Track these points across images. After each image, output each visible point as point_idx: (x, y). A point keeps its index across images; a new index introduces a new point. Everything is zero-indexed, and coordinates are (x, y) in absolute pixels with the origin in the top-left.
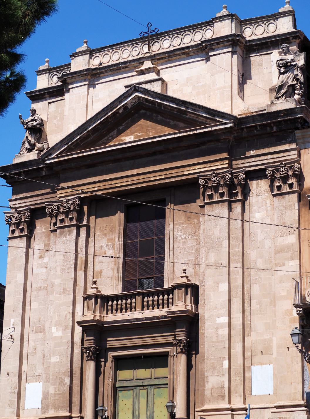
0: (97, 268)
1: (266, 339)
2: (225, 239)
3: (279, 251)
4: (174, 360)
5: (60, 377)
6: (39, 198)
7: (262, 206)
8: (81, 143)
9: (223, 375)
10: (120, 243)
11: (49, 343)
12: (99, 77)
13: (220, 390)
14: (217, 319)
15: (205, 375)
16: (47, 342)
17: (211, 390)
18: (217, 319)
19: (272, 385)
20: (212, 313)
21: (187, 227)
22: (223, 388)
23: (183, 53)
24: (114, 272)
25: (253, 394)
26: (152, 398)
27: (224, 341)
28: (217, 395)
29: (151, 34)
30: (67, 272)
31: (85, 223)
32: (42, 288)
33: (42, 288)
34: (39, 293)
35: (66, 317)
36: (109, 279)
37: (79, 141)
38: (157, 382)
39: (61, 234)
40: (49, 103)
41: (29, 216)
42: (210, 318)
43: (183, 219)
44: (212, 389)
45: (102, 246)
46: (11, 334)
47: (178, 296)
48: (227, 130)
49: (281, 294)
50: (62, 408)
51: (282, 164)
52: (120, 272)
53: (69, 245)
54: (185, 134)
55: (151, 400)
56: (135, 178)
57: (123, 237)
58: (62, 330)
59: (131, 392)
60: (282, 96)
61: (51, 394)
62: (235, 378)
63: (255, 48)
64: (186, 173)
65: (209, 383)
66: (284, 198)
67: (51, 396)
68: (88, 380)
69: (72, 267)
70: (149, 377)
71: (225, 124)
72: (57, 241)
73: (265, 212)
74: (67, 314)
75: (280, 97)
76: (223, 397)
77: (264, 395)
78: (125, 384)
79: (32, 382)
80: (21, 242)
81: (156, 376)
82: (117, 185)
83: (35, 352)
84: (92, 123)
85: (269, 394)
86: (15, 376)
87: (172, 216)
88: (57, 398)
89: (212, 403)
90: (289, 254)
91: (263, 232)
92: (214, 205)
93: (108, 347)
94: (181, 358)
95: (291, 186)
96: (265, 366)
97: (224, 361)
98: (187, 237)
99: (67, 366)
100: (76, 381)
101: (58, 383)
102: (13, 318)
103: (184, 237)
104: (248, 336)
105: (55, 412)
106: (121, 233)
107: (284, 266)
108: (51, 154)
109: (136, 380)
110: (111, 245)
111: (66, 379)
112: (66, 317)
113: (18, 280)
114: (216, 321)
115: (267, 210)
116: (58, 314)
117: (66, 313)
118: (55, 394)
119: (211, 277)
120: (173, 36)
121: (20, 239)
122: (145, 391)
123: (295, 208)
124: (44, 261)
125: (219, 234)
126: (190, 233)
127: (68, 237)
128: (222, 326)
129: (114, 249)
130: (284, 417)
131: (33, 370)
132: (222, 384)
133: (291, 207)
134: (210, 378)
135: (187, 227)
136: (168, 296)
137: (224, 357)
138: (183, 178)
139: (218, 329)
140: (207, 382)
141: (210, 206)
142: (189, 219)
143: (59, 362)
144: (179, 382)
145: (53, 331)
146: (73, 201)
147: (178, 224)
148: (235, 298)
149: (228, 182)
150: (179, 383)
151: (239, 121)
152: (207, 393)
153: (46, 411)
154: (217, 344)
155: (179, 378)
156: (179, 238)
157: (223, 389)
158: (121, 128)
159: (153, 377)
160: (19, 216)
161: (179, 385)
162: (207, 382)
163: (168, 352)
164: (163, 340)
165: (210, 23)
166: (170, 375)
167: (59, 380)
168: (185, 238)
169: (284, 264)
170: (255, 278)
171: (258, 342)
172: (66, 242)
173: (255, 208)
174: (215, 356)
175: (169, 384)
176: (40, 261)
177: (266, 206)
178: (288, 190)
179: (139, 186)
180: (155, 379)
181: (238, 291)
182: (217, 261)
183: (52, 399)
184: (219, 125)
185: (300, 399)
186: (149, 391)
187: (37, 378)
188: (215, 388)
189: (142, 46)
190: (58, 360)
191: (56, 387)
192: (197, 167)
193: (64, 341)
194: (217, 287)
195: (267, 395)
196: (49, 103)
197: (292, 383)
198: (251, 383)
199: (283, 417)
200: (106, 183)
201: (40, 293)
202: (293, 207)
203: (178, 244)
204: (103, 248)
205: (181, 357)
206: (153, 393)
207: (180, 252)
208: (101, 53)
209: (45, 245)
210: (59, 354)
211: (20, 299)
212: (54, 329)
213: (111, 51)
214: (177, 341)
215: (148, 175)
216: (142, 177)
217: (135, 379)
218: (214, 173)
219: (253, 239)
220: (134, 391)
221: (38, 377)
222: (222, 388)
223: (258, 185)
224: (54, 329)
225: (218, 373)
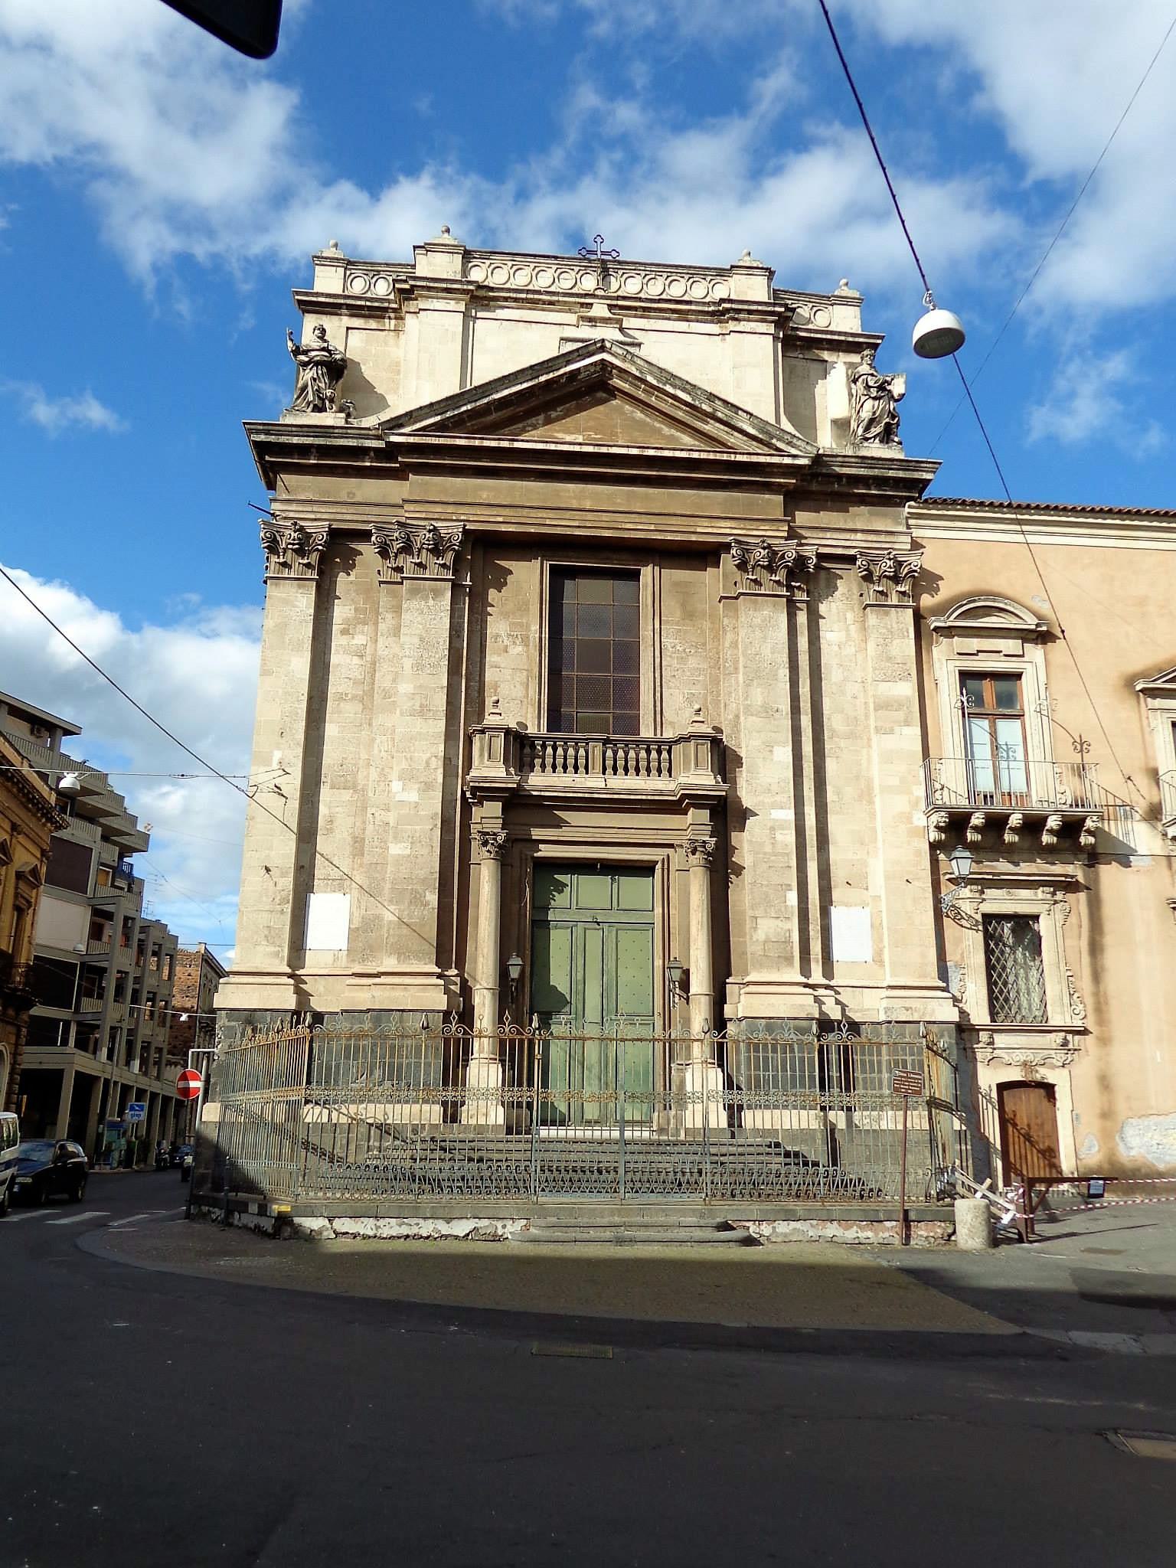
3: (884, 705)
6: (352, 509)
8: (469, 421)
11: (376, 814)
12: (487, 305)
16: (370, 811)
21: (686, 632)
27: (787, 854)
33: (349, 696)
35: (428, 763)
36: (516, 702)
37: (465, 416)
39: (414, 593)
44: (765, 942)
46: (277, 782)
48: (791, 470)
50: (419, 956)
53: (434, 619)
54: (712, 456)
58: (419, 789)
60: (875, 437)
63: (798, 343)
65: (759, 931)
66: (887, 614)
72: (405, 606)
74: (430, 758)
75: (870, 438)
76: (789, 960)
79: (322, 892)
80: (300, 591)
83: (331, 829)
84: (503, 387)
86: (283, 875)
93: (534, 837)
96: (853, 910)
98: (688, 650)
99: (432, 867)
102: (279, 749)
103: (680, 649)
105: (399, 962)
108: (401, 426)
112: (428, 763)
116: (408, 756)
117: (429, 755)
120: (646, 275)
124: (355, 642)
137: (789, 885)
138: (694, 538)
143: (409, 856)
145: (394, 790)
149: (916, 574)
154: (773, 858)
158: (554, 414)
164: (647, 837)
165: (722, 273)
168: (684, 650)
187: (342, 883)
189: (580, 274)
190: (408, 851)
192: (723, 524)
194: (771, 751)
202: (906, 634)
203: (668, 659)
208: (488, 262)
209: (356, 610)
211: (299, 711)
213: (510, 264)
216: (605, 517)
218: (763, 542)
222: (785, 942)
224: (396, 786)
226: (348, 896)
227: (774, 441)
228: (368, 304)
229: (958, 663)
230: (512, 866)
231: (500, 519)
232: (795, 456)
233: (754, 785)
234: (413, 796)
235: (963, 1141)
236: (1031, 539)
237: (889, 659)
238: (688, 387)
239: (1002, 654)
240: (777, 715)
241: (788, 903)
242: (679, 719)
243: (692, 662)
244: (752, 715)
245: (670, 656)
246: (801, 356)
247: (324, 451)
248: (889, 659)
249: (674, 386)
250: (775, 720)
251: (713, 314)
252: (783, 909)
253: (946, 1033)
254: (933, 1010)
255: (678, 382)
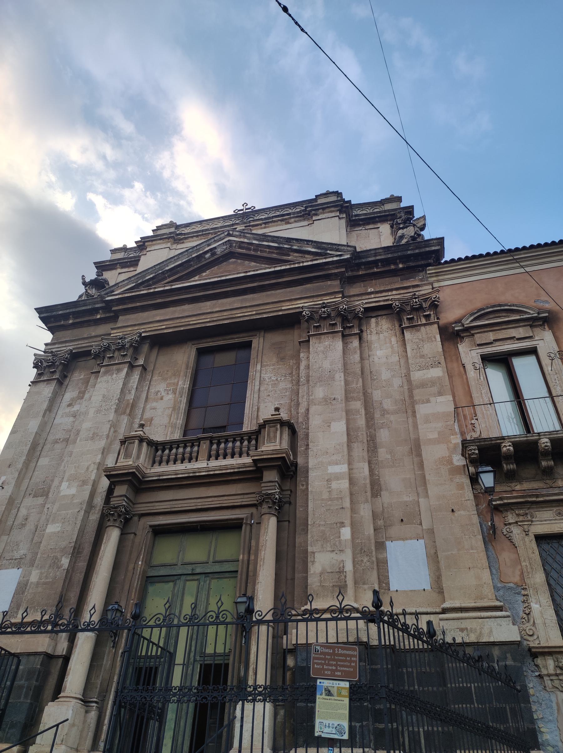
0: (147, 415)
1: (406, 502)
2: (338, 371)
4: (251, 531)
5: (53, 556)
7: (386, 343)
9: (341, 551)
10: (185, 386)
13: (337, 576)
14: (329, 468)
15: (309, 551)
17: (320, 576)
18: (329, 468)
19: (427, 573)
20: (320, 459)
21: (279, 368)
22: (343, 572)
23: (281, 220)
24: (170, 420)
25: (392, 588)
26: (205, 595)
28: (331, 585)
29: (246, 211)
30: (103, 414)
31: (141, 362)
32: (61, 440)
33: (61, 440)
34: (55, 446)
35: (88, 468)
36: (162, 427)
38: (217, 568)
40: (119, 273)
41: (67, 358)
42: (317, 467)
43: (275, 360)
44: (321, 574)
45: (159, 391)
47: (268, 435)
49: (429, 438)
51: (415, 294)
52: (179, 418)
55: (203, 600)
56: (216, 315)
57: (189, 381)
59: (171, 584)
61: (32, 583)
62: (360, 559)
64: (283, 308)
66: (418, 331)
67: (30, 587)
68: (103, 557)
69: (112, 408)
70: (204, 559)
71: (340, 255)
73: (390, 349)
74: (90, 465)
77: (415, 591)
78: (163, 572)
81: (217, 559)
82: (191, 323)
85: (424, 590)
87: (260, 357)
88: (40, 589)
89: (321, 599)
90: (435, 389)
91: (389, 371)
92: (323, 337)
94: (268, 522)
95: (427, 317)
97: (343, 528)
98: (279, 379)
100: (82, 565)
101: (47, 566)
103: (274, 379)
104: (377, 496)
106: (187, 376)
107: (429, 403)
109: (181, 565)
110: (171, 390)
111: (63, 559)
112: (88, 468)
113: (29, 429)
114: (328, 470)
115: (392, 347)
117: (90, 463)
118: (38, 584)
119: (318, 415)
121: (47, 384)
122: (195, 583)
123: (436, 340)
125: (329, 367)
126: (283, 375)
127: (115, 375)
128: (338, 477)
129: (175, 394)
130: (469, 628)
131: (13, 551)
132: (339, 565)
133: (430, 339)
134: (316, 555)
135: (279, 368)
136: (249, 442)
137: (343, 523)
138: (280, 313)
139: (330, 481)
140: (312, 562)
141: (317, 338)
142: (283, 360)
143: (59, 532)
144: (263, 561)
146: (131, 338)
147: (267, 365)
148: (355, 442)
150: (263, 562)
151: (357, 255)
152: (313, 581)
153: (13, 615)
155: (264, 554)
156: (268, 380)
157: (343, 574)
159: (211, 559)
160: (54, 359)
161: (263, 564)
162: (312, 562)
163: (242, 519)
166: (243, 554)
167: (53, 559)
168: (277, 379)
169: (429, 400)
170: (381, 422)
171: (393, 506)
172: (110, 381)
173: (376, 345)
174: (325, 521)
175: (239, 572)
176: (67, 410)
177: (391, 343)
178: (424, 321)
179: (221, 323)
180: (215, 564)
181: (359, 434)
182: (328, 396)
183: (31, 591)
184: (333, 257)
185: (490, 597)
186: (202, 583)
188: (328, 572)
190: (59, 529)
191: (43, 571)
192: (299, 302)
193: (75, 501)
194: (329, 426)
195: (419, 590)
196: (119, 273)
197: (469, 568)
198: (387, 571)
199: (467, 629)
200: (178, 321)
201: (57, 446)
202: (434, 339)
203: (266, 386)
204: (159, 393)
205: (269, 519)
206: (209, 587)
207: (269, 395)
210: (63, 521)
212: (65, 485)
214: (263, 496)
215: (235, 312)
216: (225, 313)
217: (180, 563)
219: (375, 377)
220: (175, 585)
221: (17, 561)
222: (340, 572)
223: (377, 323)
225: (331, 547)
226: (20, 570)
227: (328, 252)
228: (129, 260)
229: (479, 351)
230: (135, 534)
231: (164, 327)
232: (340, 255)
233: (315, 450)
234: (73, 491)
235: (421, 724)
236: (528, 269)
237: (422, 356)
238: (275, 239)
239: (515, 339)
240: (334, 402)
241: (342, 538)
242: (267, 413)
243: (282, 385)
244: (315, 405)
245: (267, 384)
246: (364, 229)
247: (76, 315)
248: (422, 356)
249: (268, 241)
250: (332, 405)
251: (303, 216)
252: (337, 543)
253: (509, 655)
254: (491, 631)
255: (270, 238)
